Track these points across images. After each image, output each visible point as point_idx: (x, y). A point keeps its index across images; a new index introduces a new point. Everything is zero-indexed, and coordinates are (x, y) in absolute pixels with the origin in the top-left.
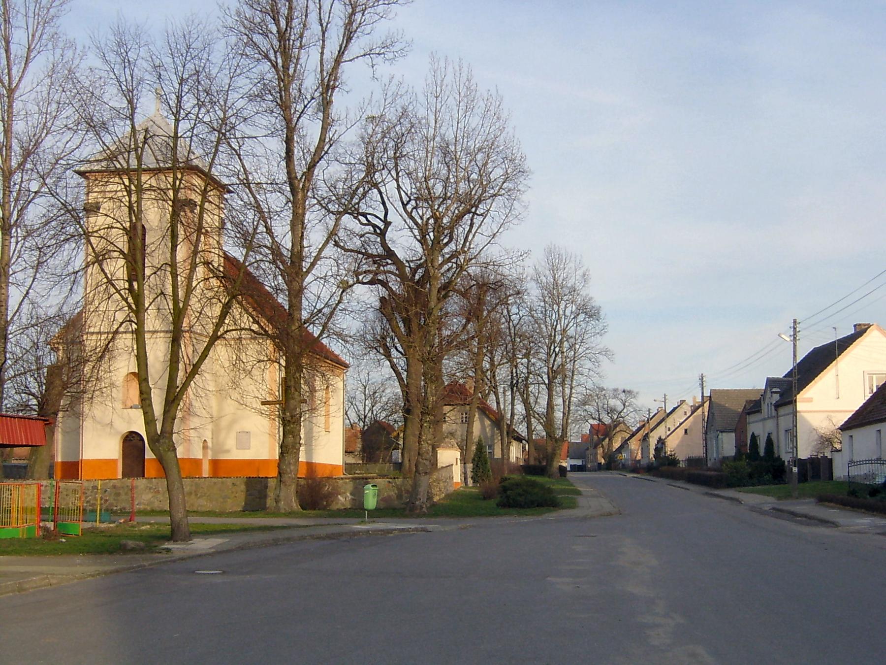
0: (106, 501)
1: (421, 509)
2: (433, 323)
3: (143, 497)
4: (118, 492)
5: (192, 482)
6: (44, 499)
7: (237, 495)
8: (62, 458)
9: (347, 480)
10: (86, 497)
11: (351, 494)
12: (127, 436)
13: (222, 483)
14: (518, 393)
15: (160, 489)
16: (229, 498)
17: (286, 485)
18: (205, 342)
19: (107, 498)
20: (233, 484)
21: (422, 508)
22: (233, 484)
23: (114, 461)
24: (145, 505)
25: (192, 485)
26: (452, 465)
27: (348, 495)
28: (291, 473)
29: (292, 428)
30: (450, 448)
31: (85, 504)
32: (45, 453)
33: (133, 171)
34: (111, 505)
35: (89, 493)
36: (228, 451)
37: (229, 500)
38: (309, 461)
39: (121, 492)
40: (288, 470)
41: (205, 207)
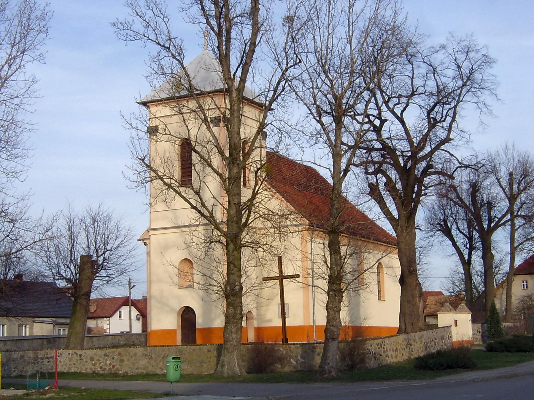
0: (114, 366)
1: (329, 373)
2: (336, 197)
3: (141, 362)
4: (122, 358)
5: (177, 349)
6: (71, 365)
7: (211, 360)
8: (8, 332)
9: (299, 345)
10: (100, 363)
11: (301, 358)
12: (184, 311)
13: (200, 349)
14: (342, 254)
15: (153, 356)
16: (205, 363)
17: (228, 352)
18: (464, 250)
19: (115, 364)
20: (208, 350)
21: (330, 372)
22: (208, 350)
23: (174, 331)
24: (142, 369)
25: (176, 352)
26: (451, 326)
27: (299, 358)
28: (232, 341)
29: (232, 300)
30: (448, 311)
31: (99, 369)
32: (79, 327)
33: (167, 100)
34: (117, 369)
35: (102, 360)
36: (270, 321)
37: (204, 364)
38: (357, 324)
39: (124, 358)
40: (230, 338)
41: (358, 152)
